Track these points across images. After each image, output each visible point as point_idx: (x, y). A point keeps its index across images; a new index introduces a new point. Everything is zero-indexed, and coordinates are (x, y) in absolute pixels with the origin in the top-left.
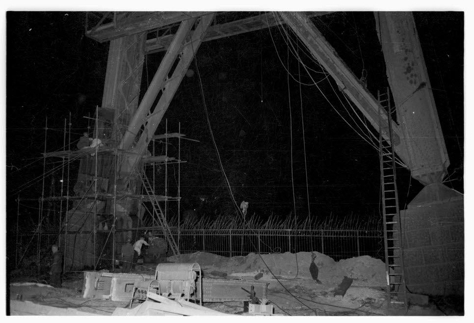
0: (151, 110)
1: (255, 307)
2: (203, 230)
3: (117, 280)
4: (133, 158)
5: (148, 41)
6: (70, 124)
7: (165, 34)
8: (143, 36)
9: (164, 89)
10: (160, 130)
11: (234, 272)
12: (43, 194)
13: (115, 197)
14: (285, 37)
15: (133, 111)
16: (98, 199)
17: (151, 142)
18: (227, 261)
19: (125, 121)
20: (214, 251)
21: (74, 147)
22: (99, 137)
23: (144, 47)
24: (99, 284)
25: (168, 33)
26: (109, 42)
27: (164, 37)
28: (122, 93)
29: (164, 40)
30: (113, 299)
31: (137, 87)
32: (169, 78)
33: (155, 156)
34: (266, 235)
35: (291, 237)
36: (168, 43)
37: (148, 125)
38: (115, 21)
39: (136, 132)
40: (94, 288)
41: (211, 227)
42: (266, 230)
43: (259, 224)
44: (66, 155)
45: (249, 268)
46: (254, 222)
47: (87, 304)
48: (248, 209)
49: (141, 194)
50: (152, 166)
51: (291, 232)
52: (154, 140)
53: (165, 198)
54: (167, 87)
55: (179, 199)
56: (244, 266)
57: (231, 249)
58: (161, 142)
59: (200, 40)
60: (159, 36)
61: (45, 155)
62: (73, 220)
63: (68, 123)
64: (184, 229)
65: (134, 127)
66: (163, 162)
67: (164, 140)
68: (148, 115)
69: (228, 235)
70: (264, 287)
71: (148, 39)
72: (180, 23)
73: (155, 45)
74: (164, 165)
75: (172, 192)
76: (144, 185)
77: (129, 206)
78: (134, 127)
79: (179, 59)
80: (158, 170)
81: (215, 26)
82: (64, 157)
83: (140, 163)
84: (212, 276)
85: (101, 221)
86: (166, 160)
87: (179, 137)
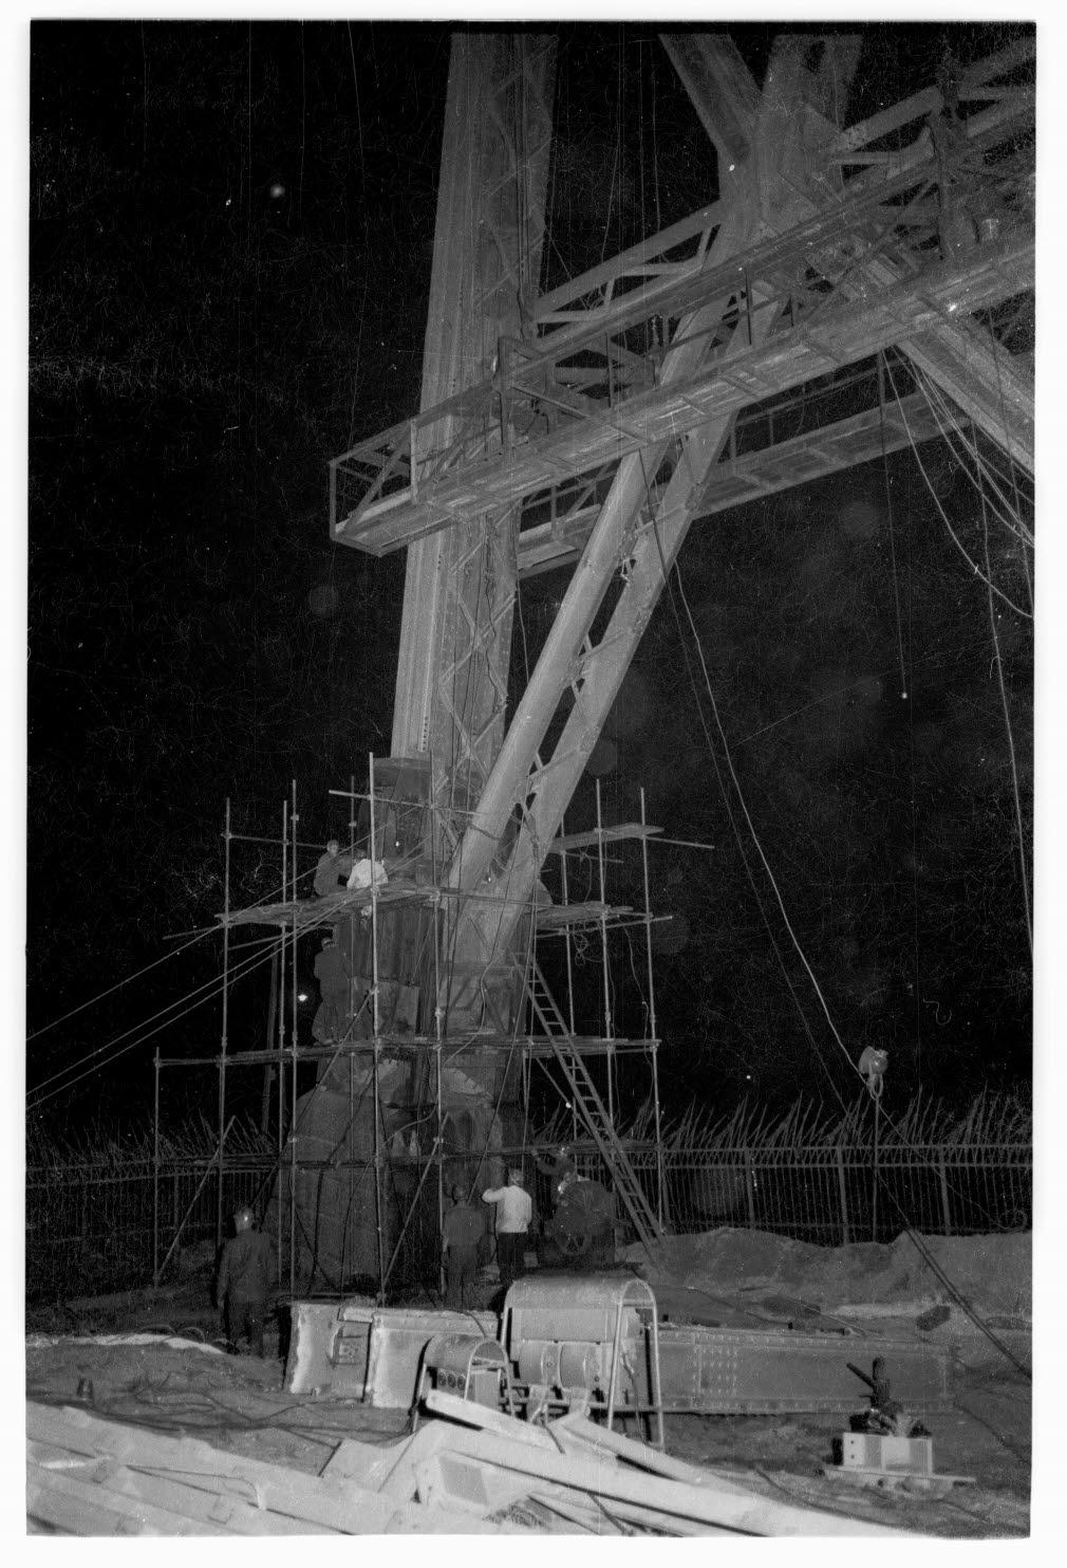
0: (541, 752)
1: (868, 1443)
2: (745, 1148)
3: (393, 1337)
4: (492, 911)
5: (524, 536)
6: (295, 818)
7: (577, 506)
8: (505, 523)
9: (581, 683)
10: (577, 817)
11: (845, 1300)
12: (224, 1044)
13: (438, 1048)
14: (971, 465)
15: (487, 764)
16: (388, 1052)
17: (553, 860)
18: (826, 1260)
19: (465, 797)
20: (780, 1225)
21: (307, 892)
22: (386, 853)
23: (512, 553)
24: (342, 1347)
25: (588, 503)
26: (404, 550)
27: (577, 514)
28: (449, 707)
29: (573, 525)
30: (378, 1402)
31: (499, 682)
32: (593, 646)
33: (570, 903)
34: (966, 1165)
35: (947, 1169)
36: (585, 532)
37: (537, 804)
38: (413, 483)
39: (499, 829)
40: (324, 1358)
41: (772, 1140)
42: (965, 1146)
43: (710, 1128)
44: (288, 916)
45: (902, 1287)
46: (746, 1121)
47: (288, 1418)
48: (889, 1074)
49: (528, 1033)
50: (564, 938)
51: (704, 1162)
52: (563, 853)
53: (606, 1044)
54: (589, 675)
55: (653, 1045)
56: (883, 1280)
57: (845, 1217)
58: (583, 856)
59: (686, 512)
60: (559, 515)
61: (227, 920)
62: (316, 1126)
63: (290, 813)
64: (734, 1146)
65: (489, 812)
66: (593, 924)
67: (593, 850)
68: (534, 769)
69: (833, 1165)
70: (943, 1361)
71: (524, 528)
72: (616, 464)
73: (545, 545)
74: (598, 934)
75: (630, 1024)
76: (535, 1004)
77: (492, 1074)
78: (489, 812)
79: (622, 583)
80: (579, 951)
81: (734, 460)
82: (283, 924)
83: (520, 929)
84: (769, 1316)
85: (396, 1127)
86: (604, 918)
87: (644, 837)
